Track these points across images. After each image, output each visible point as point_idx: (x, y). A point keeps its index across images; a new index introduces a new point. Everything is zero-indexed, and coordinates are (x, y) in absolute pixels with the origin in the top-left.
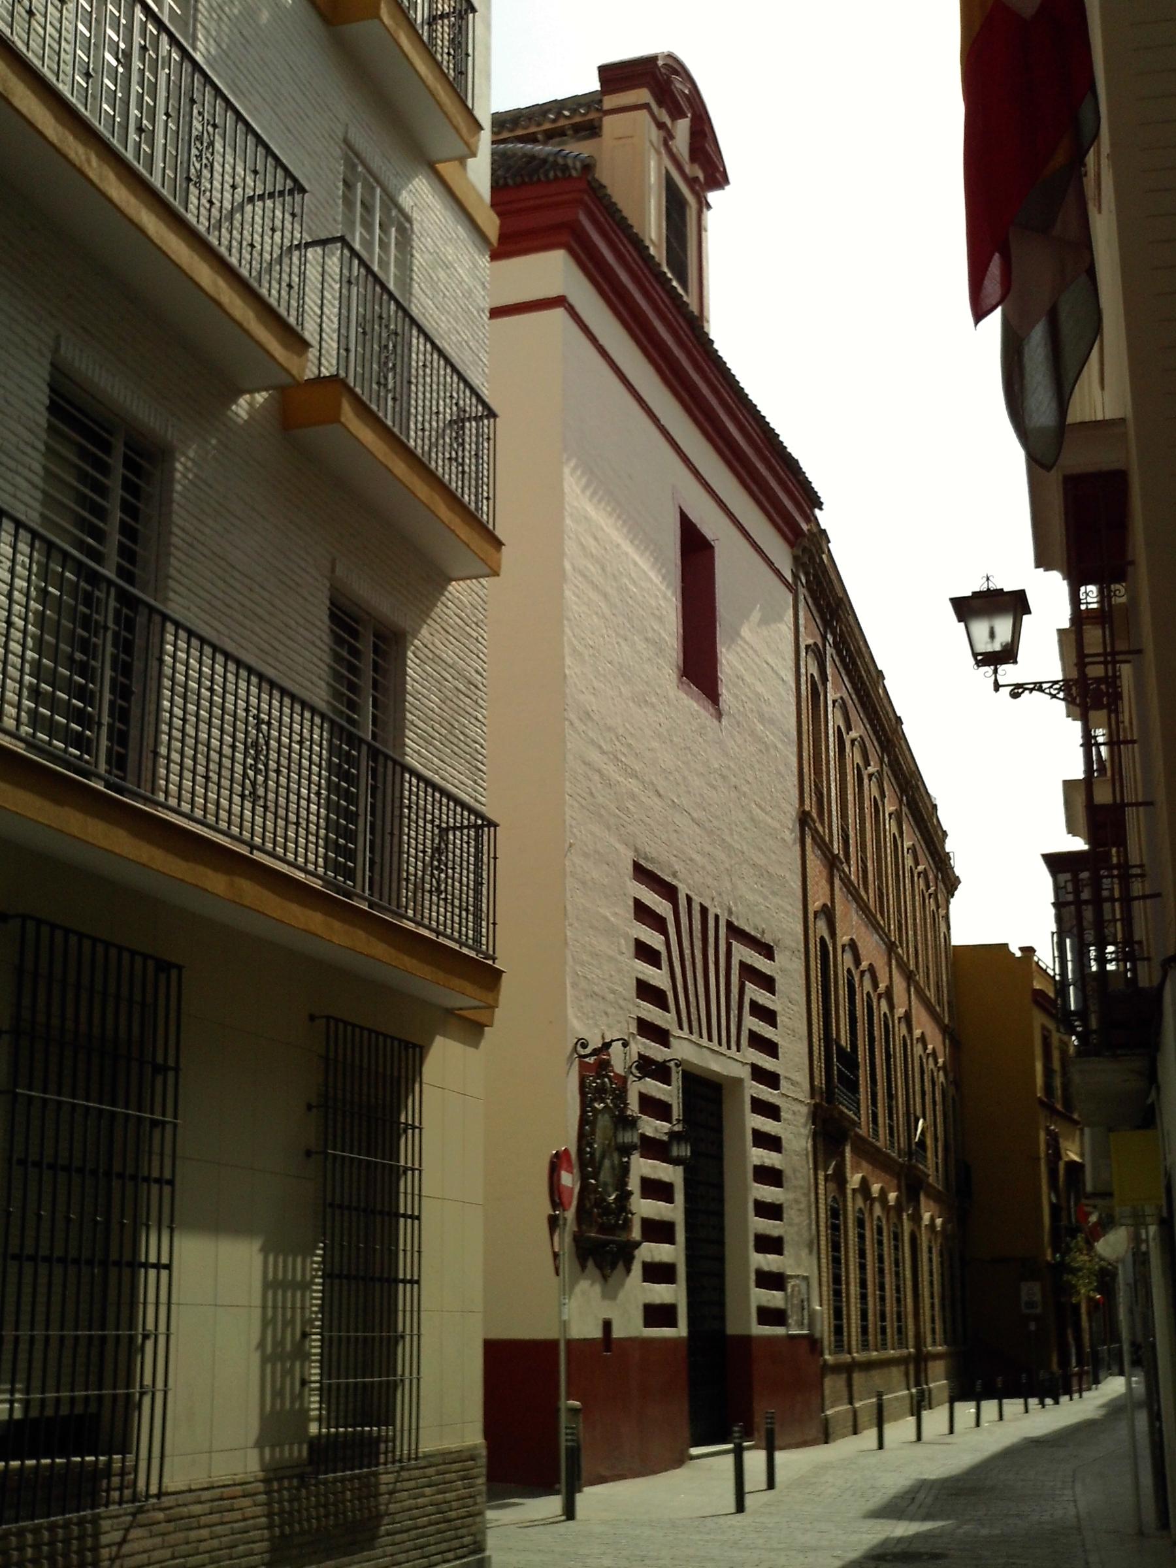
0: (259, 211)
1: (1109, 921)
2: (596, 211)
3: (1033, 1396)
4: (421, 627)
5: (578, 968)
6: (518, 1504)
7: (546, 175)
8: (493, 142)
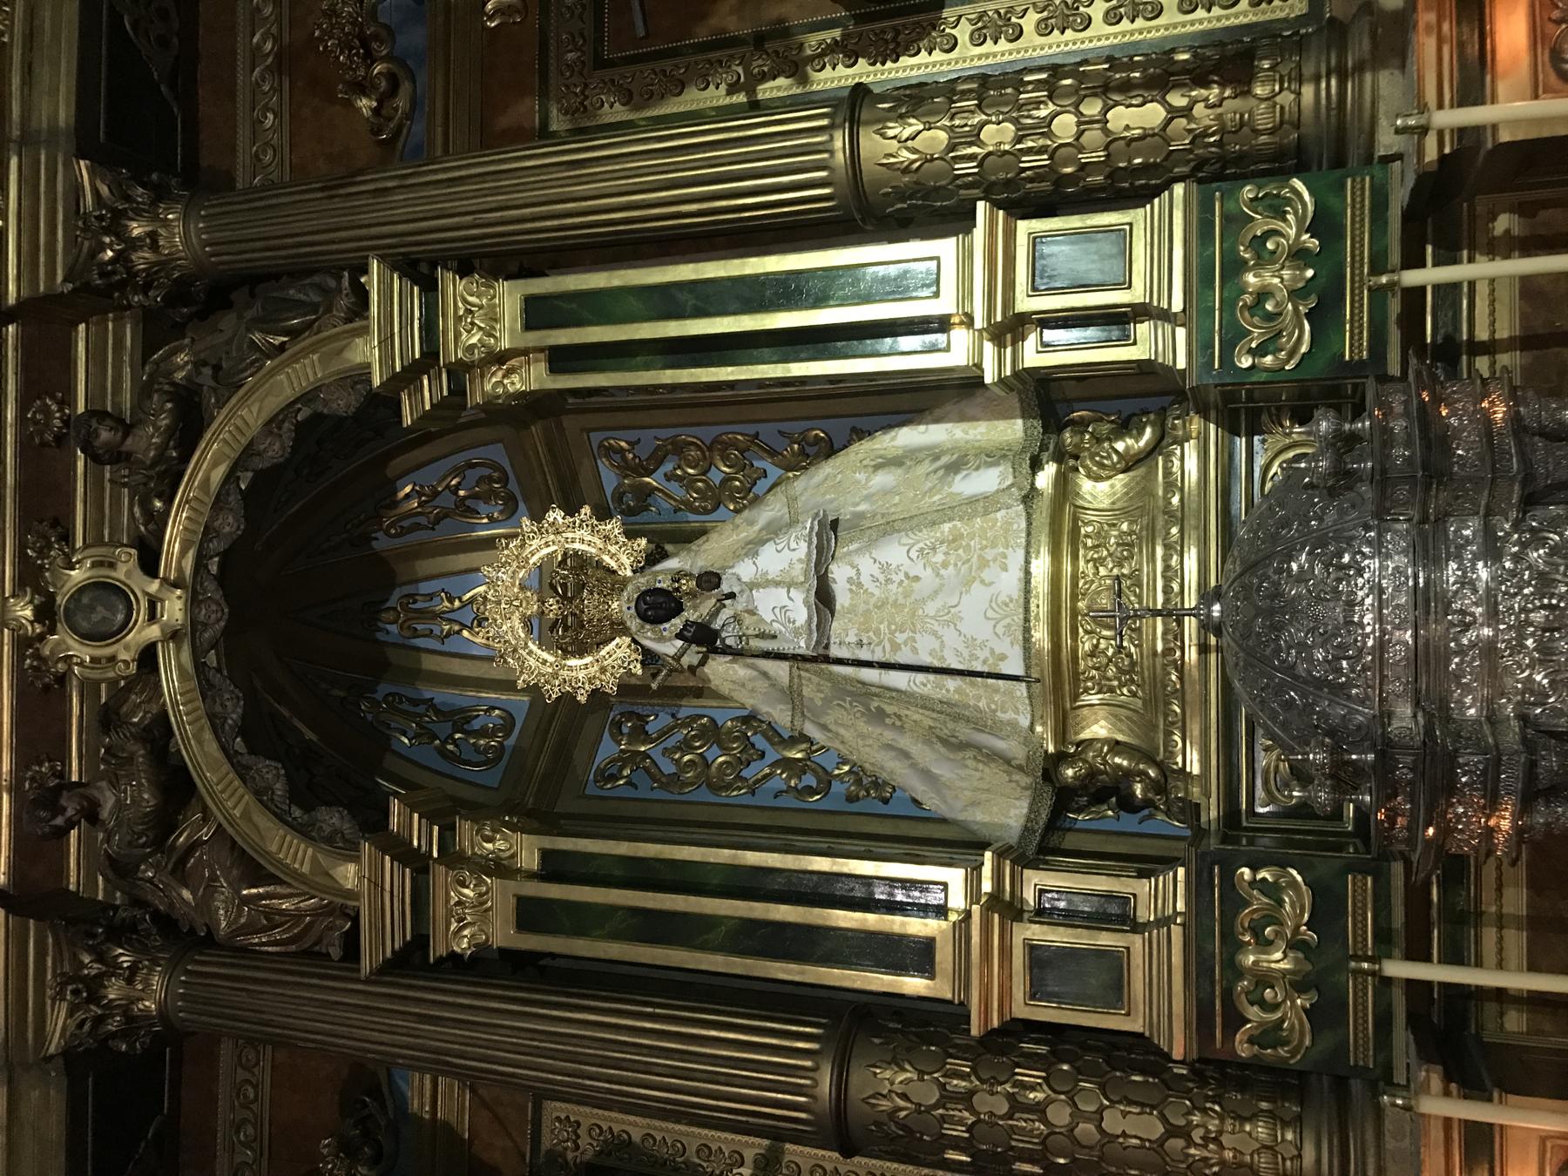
3: (1483, 343)
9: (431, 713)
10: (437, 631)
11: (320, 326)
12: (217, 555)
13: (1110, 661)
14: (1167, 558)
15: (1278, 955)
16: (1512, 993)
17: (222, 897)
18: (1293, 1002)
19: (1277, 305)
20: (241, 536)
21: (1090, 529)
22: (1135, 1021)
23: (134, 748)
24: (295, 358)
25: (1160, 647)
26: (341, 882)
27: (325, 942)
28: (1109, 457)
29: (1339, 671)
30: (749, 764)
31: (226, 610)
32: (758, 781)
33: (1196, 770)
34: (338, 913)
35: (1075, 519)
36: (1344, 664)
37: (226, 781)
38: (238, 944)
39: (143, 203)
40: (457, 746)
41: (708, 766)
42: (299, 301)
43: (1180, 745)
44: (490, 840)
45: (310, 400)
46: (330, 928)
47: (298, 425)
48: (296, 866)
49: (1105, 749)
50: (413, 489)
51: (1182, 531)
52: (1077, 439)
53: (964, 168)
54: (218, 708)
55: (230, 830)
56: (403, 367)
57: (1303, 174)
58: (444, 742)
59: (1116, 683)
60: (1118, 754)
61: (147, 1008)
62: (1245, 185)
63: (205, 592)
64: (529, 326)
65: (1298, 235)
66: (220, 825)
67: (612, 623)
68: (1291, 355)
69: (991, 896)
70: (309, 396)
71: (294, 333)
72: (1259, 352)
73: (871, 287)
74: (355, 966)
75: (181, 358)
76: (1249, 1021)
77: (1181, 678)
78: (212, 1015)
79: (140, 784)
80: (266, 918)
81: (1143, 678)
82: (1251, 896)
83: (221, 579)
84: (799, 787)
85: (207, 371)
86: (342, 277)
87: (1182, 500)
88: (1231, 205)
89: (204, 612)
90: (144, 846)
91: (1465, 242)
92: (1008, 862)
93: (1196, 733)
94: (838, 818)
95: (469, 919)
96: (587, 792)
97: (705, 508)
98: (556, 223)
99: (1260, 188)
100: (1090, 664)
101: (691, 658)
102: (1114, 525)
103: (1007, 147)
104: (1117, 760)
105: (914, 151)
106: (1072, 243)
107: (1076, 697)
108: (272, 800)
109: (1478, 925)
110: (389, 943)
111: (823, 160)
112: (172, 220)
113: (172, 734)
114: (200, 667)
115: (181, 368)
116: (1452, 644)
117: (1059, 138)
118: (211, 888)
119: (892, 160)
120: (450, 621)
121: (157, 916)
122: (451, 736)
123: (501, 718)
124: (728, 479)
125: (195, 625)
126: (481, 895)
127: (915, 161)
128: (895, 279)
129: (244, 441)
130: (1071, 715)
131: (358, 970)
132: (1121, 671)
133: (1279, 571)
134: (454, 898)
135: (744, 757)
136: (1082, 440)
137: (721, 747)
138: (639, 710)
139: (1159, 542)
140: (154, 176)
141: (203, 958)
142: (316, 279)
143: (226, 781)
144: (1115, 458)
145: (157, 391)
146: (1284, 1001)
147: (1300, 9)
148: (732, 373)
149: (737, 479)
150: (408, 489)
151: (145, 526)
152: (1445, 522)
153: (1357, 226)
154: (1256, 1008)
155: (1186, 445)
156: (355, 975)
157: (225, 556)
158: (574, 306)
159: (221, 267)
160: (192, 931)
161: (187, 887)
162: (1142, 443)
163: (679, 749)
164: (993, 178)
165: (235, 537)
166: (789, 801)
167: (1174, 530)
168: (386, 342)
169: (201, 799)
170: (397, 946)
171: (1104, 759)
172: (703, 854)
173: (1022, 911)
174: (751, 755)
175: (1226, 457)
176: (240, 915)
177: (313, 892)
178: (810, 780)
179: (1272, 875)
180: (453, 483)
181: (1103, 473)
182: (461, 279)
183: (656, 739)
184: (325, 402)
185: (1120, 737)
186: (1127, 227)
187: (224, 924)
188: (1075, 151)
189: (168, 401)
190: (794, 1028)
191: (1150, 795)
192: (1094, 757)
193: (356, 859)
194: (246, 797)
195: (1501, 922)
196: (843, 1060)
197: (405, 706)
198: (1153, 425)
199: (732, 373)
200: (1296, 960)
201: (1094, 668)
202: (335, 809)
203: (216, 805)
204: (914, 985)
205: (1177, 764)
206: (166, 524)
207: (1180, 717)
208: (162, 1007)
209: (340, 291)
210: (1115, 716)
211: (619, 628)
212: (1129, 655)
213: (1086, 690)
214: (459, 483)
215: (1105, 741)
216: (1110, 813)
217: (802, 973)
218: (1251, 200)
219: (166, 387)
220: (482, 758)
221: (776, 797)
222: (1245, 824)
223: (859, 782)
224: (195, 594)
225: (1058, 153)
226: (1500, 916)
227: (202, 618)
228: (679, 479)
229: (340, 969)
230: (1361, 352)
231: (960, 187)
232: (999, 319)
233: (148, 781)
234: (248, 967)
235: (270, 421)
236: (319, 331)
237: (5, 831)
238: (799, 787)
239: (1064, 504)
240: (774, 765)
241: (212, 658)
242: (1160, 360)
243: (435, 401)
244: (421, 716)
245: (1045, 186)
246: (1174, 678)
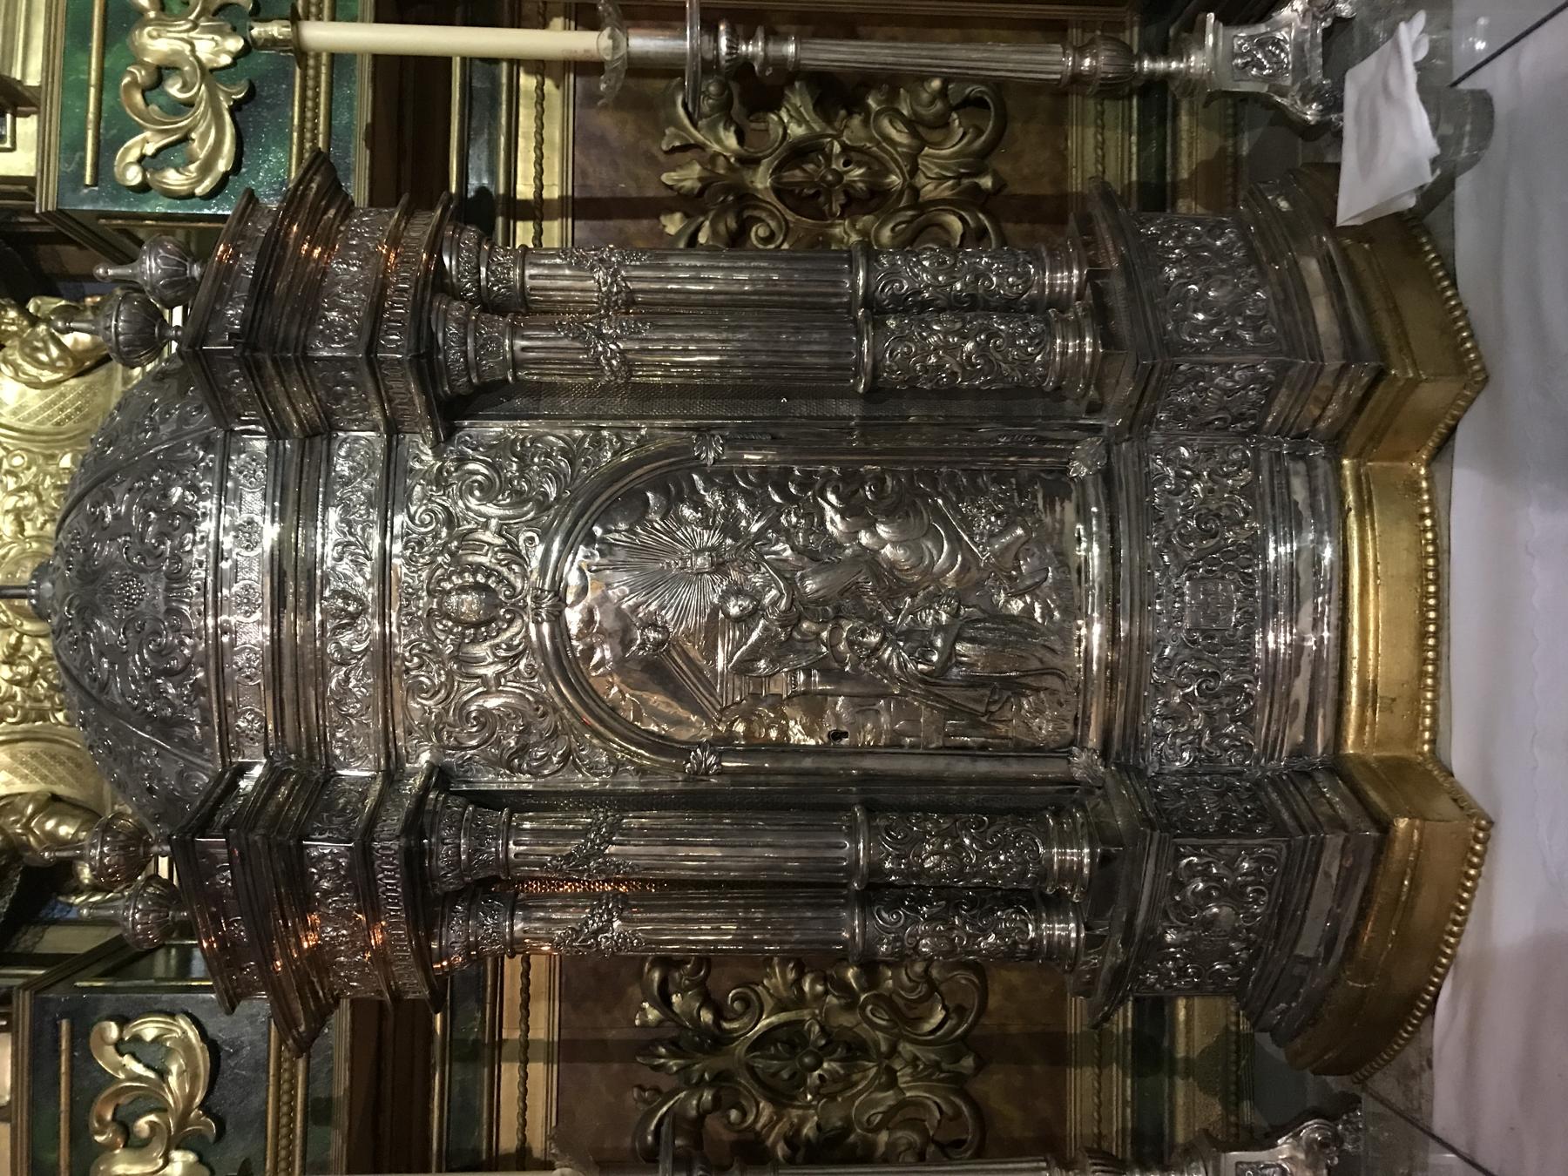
0: (730, 697)
1: (429, 811)
2: (708, 358)
3: (526, 202)
4: (556, 219)
5: (352, 539)
6: (1351, 219)
7: (1208, 326)
8: (319, 19)
109: (494, 1064)
152: (330, 440)
170: (1121, 1011)
185: (61, 790)
195: (525, 1052)
210: (53, 757)
226: (526, 1044)
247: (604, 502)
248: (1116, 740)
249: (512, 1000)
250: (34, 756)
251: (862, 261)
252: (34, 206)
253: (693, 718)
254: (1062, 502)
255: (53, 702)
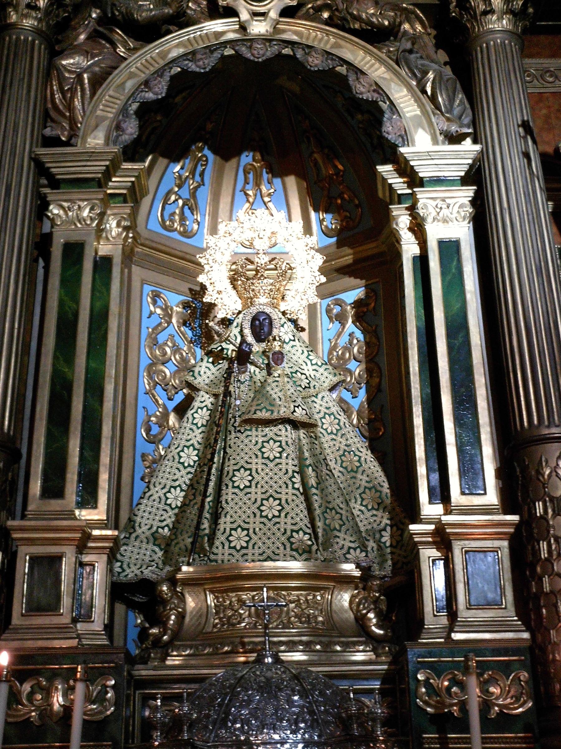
9: (195, 184)
10: (247, 187)
11: (438, 115)
12: (235, 51)
13: (236, 611)
14: (301, 643)
15: (61, 699)
16: (499, 466)
17: (81, 61)
18: (33, 711)
19: (456, 693)
20: (306, 68)
21: (319, 598)
22: (18, 619)
23: (174, 7)
24: (418, 101)
25: (246, 640)
26: (92, 136)
27: (53, 125)
28: (364, 608)
29: (234, 722)
30: (165, 390)
31: (260, 60)
32: (154, 396)
33: (168, 663)
34: (72, 133)
35: (325, 589)
36: (238, 726)
37: (153, 62)
38: (52, 71)
39: (513, 5)
40: (174, 202)
41: (163, 364)
42: (454, 100)
43: (184, 653)
44: (118, 225)
45: (392, 110)
46: (63, 128)
47: (223, 57)
48: (101, 107)
49: (180, 610)
50: (341, 170)
51: (318, 651)
52: (376, 588)
53: (539, 508)
54: (199, 56)
55: (123, 65)
56: (449, 534)
57: (218, 158)
58: (176, 193)
59: (222, 616)
60: (177, 617)
61: (10, 17)
62: (528, 674)
63: (270, 47)
64: (442, 244)
65: (498, 705)
66: (125, 59)
67: (252, 298)
68: (426, 703)
69: (90, 535)
70: (394, 109)
71: (433, 99)
72: (427, 683)
73: (467, 453)
74: (39, 144)
75: (419, 28)
76: (21, 685)
77: (227, 653)
78: (8, 55)
79: (151, 10)
80: (69, 89)
81: (225, 631)
82: (97, 686)
83: (279, 56)
84: (150, 423)
85: (409, 46)
86: (469, 128)
87: (337, 651)
88: (517, 665)
89: (259, 46)
90: (113, 13)
91: (370, 282)
92: (111, 545)
93: (193, 662)
94: (131, 450)
95: (70, 214)
96: (145, 286)
97: (332, 359)
98: (504, 258)
99: (526, 682)
100: (233, 599)
101: (314, 491)
102: (321, 613)
103: (552, 532)
104: (173, 617)
105: (550, 475)
106: (494, 573)
107: (212, 592)
108: (142, 91)
110: (54, 165)
111: (544, 422)
112: (502, 23)
113: (181, 28)
114: (225, 44)
115: (413, 27)
116: (233, 709)
117: (558, 563)
118: (87, 54)
119: (544, 464)
120: (255, 195)
121: (67, 20)
122: (180, 197)
123: (192, 229)
124: (350, 372)
125: (250, 42)
126: (84, 220)
127: (543, 477)
128: (472, 468)
129: (365, 69)
130: (200, 589)
131: (37, 147)
132: (230, 617)
133: (293, 690)
134: (83, 204)
135: (169, 387)
136: (376, 592)
137: (176, 372)
138: (497, 677)
139: (311, 638)
140: (531, 10)
141: (42, 50)
142: (469, 111)
143: (153, 62)
144: (364, 612)
145: (396, 14)
146: (34, 706)
147: (425, 206)
148: (420, 447)
149: (351, 379)
150: (340, 167)
151: (312, 8)
153: (504, 740)
154: (29, 689)
155: (372, 653)
156: (34, 145)
157: (293, 58)
158: (454, 270)
159: (474, 53)
160: (59, 42)
161: (87, 39)
162: (374, 628)
163: (174, 345)
164: (534, 525)
165: (306, 64)
166: (141, 416)
167: (318, 647)
168: (429, 155)
169: (142, 47)
170: (53, 170)
171: (174, 609)
172: (412, 343)
173: (81, 554)
174: (171, 392)
175: (366, 676)
176: (70, 72)
177: (85, 119)
178: (155, 430)
179: (110, 698)
180: (346, 196)
181: (354, 606)
182: (470, 201)
183: (180, 330)
184: (390, 119)
185: (187, 619)
186: (503, 606)
187: (64, 62)
188: (550, 573)
189: (389, 22)
190: (7, 414)
191: (151, 638)
192: (174, 603)
193: (107, 143)
194: (143, 75)
196: (537, 441)
197: (200, 169)
198: (385, 635)
199: (41, 410)
200: (58, 713)
201: (231, 602)
202: (137, 130)
203: (139, 56)
204: (36, 487)
205: (172, 651)
206: (312, 21)
207: (202, 653)
208: (13, 26)
209: (460, 127)
210: (200, 616)
211: (248, 302)
212: (239, 623)
213: (217, 598)
214: (345, 200)
215: (184, 609)
216: (139, 621)
217: (415, 374)
218: (519, 678)
219: (398, 20)
220: (166, 217)
221: (144, 408)
222: (137, 692)
223: (154, 462)
224: (270, 41)
225: (544, 521)
227: (256, 45)
228: (351, 343)
229: (38, 135)
230: (428, 744)
231: (529, 505)
232: (448, 530)
233: (154, 15)
234: (26, 191)
235: (376, 84)
236: (434, 114)
237: (2, 376)
238: (150, 423)
239: (335, 582)
240: (164, 406)
241: (229, 52)
242: (110, 184)
243: (393, 186)
244: (193, 178)
245: (530, 558)
246: (226, 648)
247: (531, 266)
248: (234, 584)
249: (420, 447)
250: (200, 609)
251: (473, 21)
252: (394, 204)
253: (108, 45)
254: (404, 183)
255: (223, 618)
